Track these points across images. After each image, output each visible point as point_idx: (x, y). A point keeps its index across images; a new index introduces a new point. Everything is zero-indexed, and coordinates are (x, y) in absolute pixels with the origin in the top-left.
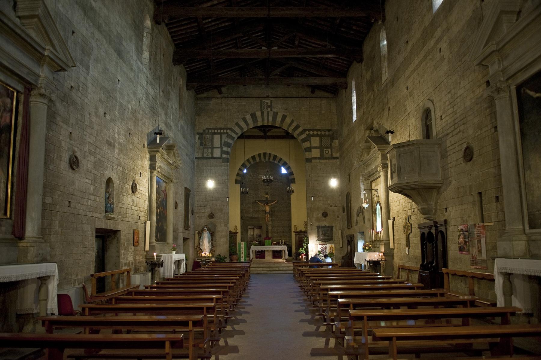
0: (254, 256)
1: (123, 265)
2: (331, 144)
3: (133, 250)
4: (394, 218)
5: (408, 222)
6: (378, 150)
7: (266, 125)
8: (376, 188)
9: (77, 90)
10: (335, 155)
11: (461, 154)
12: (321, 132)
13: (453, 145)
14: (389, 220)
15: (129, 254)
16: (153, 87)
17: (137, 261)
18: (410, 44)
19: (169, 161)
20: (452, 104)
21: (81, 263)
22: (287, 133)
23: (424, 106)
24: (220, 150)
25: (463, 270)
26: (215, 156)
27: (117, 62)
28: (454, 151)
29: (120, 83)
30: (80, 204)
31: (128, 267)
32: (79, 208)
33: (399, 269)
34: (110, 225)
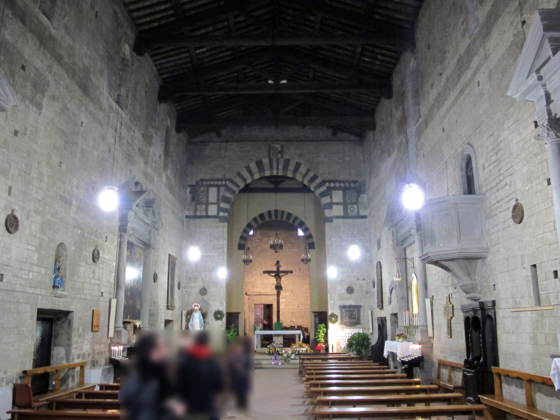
0: (259, 344)
1: (76, 357)
2: (357, 200)
3: (91, 337)
4: (433, 296)
5: (450, 302)
7: (275, 176)
9: (22, 134)
10: (362, 213)
11: (510, 213)
13: (499, 201)
14: (426, 300)
15: (84, 342)
16: (129, 129)
17: (96, 351)
18: (444, 77)
19: (146, 221)
20: (495, 149)
21: (12, 356)
22: (305, 186)
23: (463, 151)
24: (216, 206)
25: (517, 370)
26: (209, 214)
27: (81, 101)
28: (501, 210)
29: (84, 125)
30: (18, 277)
31: (82, 359)
32: (15, 283)
33: (439, 364)
34: (59, 305)
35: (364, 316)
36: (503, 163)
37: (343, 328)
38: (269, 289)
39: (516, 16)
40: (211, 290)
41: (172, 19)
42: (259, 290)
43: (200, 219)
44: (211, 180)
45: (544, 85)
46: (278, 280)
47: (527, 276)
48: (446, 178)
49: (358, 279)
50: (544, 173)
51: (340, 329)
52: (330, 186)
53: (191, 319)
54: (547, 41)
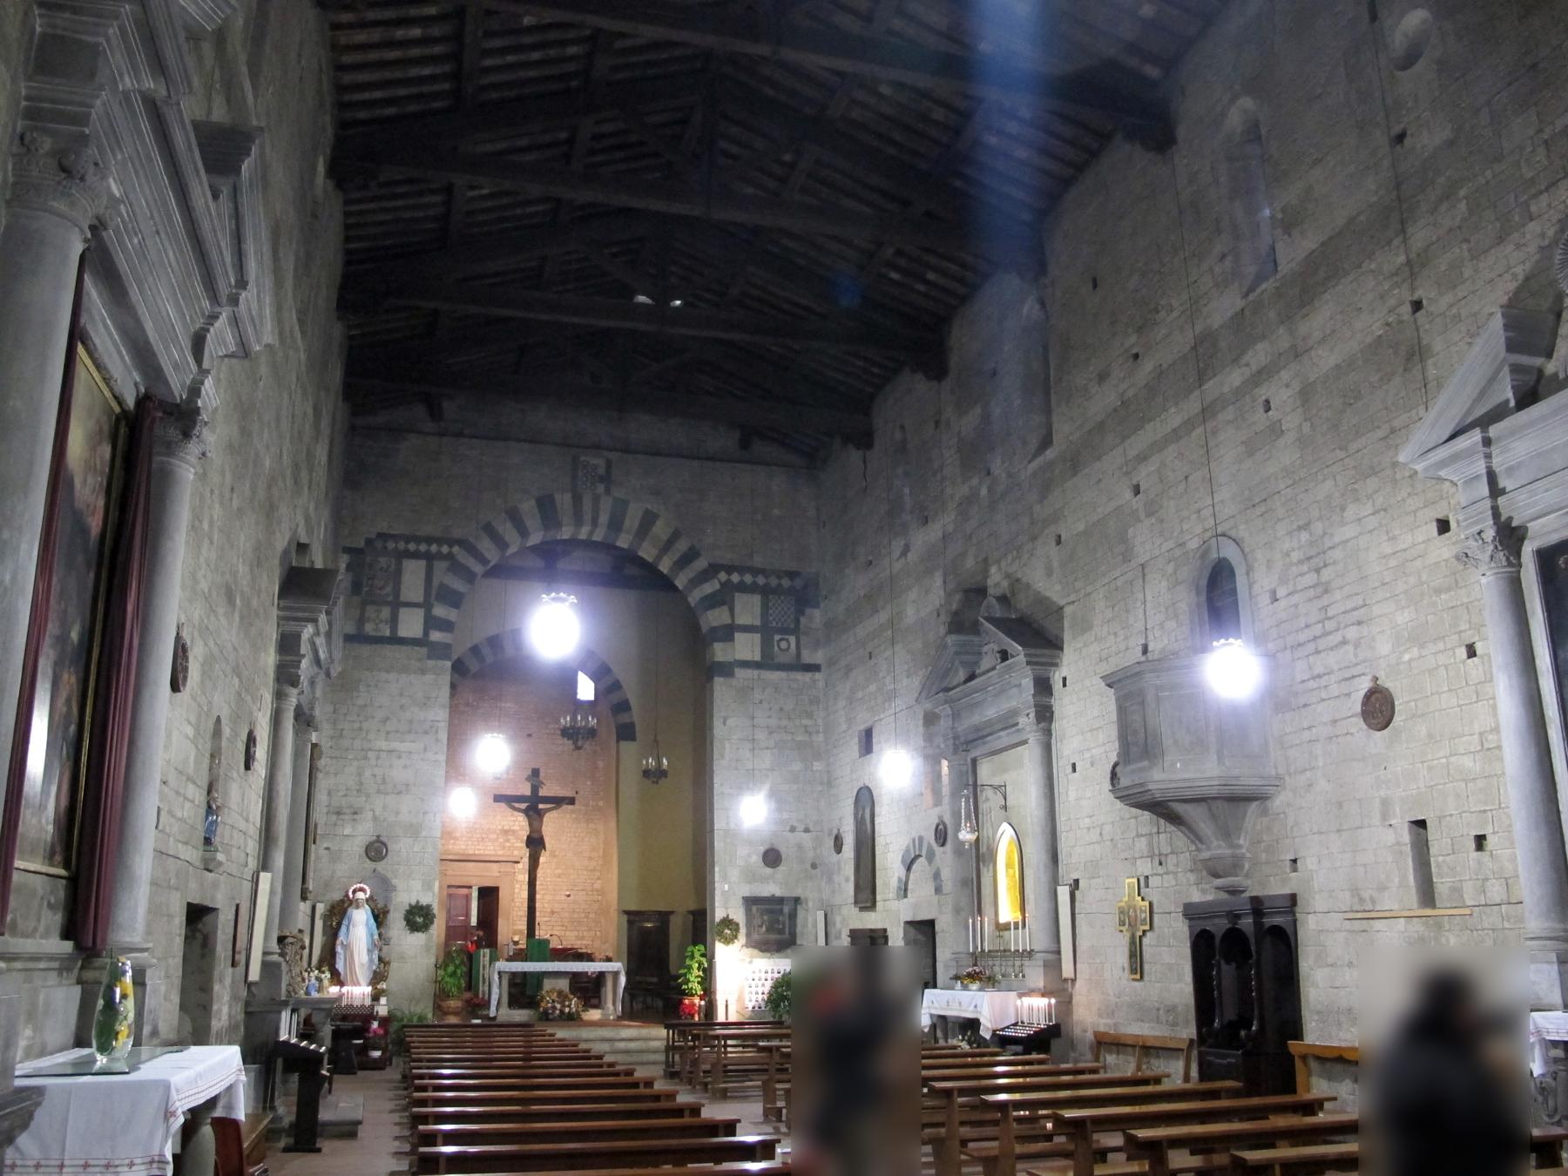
2: (797, 621)
4: (1077, 881)
5: (1139, 895)
6: (1028, 663)
8: (996, 781)
10: (807, 657)
12: (766, 577)
13: (1319, 676)
18: (1147, 366)
20: (1316, 560)
24: (420, 612)
28: (1324, 695)
35: (805, 926)
36: (1338, 595)
37: (752, 957)
38: (490, 844)
39: (1397, 285)
40: (401, 847)
41: (436, 105)
42: (463, 847)
43: (374, 646)
44: (408, 539)
45: (1488, 456)
46: (536, 824)
47: (1398, 844)
48: (1139, 604)
49: (793, 829)
50: (1460, 632)
51: (744, 960)
52: (729, 581)
53: (343, 928)
54: (1506, 369)
